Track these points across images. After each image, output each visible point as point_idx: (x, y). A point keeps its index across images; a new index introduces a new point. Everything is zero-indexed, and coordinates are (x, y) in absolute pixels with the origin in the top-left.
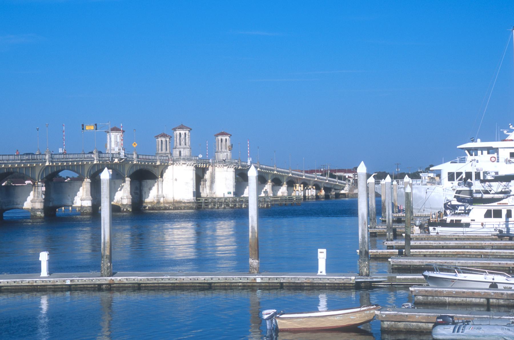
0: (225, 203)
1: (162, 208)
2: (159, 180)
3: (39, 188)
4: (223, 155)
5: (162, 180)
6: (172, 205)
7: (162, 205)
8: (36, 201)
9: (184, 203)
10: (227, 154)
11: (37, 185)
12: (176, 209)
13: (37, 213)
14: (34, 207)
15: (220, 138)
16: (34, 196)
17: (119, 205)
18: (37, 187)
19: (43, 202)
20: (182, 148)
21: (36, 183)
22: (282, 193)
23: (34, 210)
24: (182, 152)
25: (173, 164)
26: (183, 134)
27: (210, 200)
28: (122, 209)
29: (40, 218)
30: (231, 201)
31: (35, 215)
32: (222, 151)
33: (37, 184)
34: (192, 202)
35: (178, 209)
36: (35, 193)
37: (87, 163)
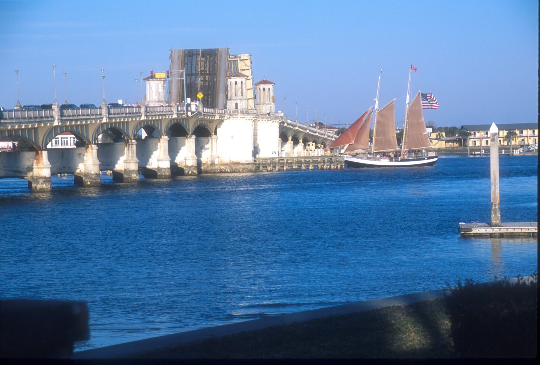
0: (287, 164)
1: (218, 170)
2: (213, 138)
3: (133, 146)
4: (266, 108)
5: (217, 138)
6: (228, 167)
7: (217, 167)
8: (130, 162)
9: (243, 164)
10: (271, 107)
11: (131, 143)
12: (233, 172)
13: (132, 175)
14: (128, 168)
15: (262, 86)
16: (128, 156)
17: (182, 167)
18: (131, 145)
19: (97, 165)
20: (239, 99)
21: (130, 141)
22: (298, 153)
23: (128, 172)
24: (238, 105)
25: (229, 118)
26: (239, 83)
27: (269, 160)
28: (187, 171)
29: (135, 181)
30: (295, 162)
31: (130, 178)
32: (265, 103)
33: (131, 141)
34: (252, 164)
35: (236, 172)
36: (129, 153)
37: (132, 120)
